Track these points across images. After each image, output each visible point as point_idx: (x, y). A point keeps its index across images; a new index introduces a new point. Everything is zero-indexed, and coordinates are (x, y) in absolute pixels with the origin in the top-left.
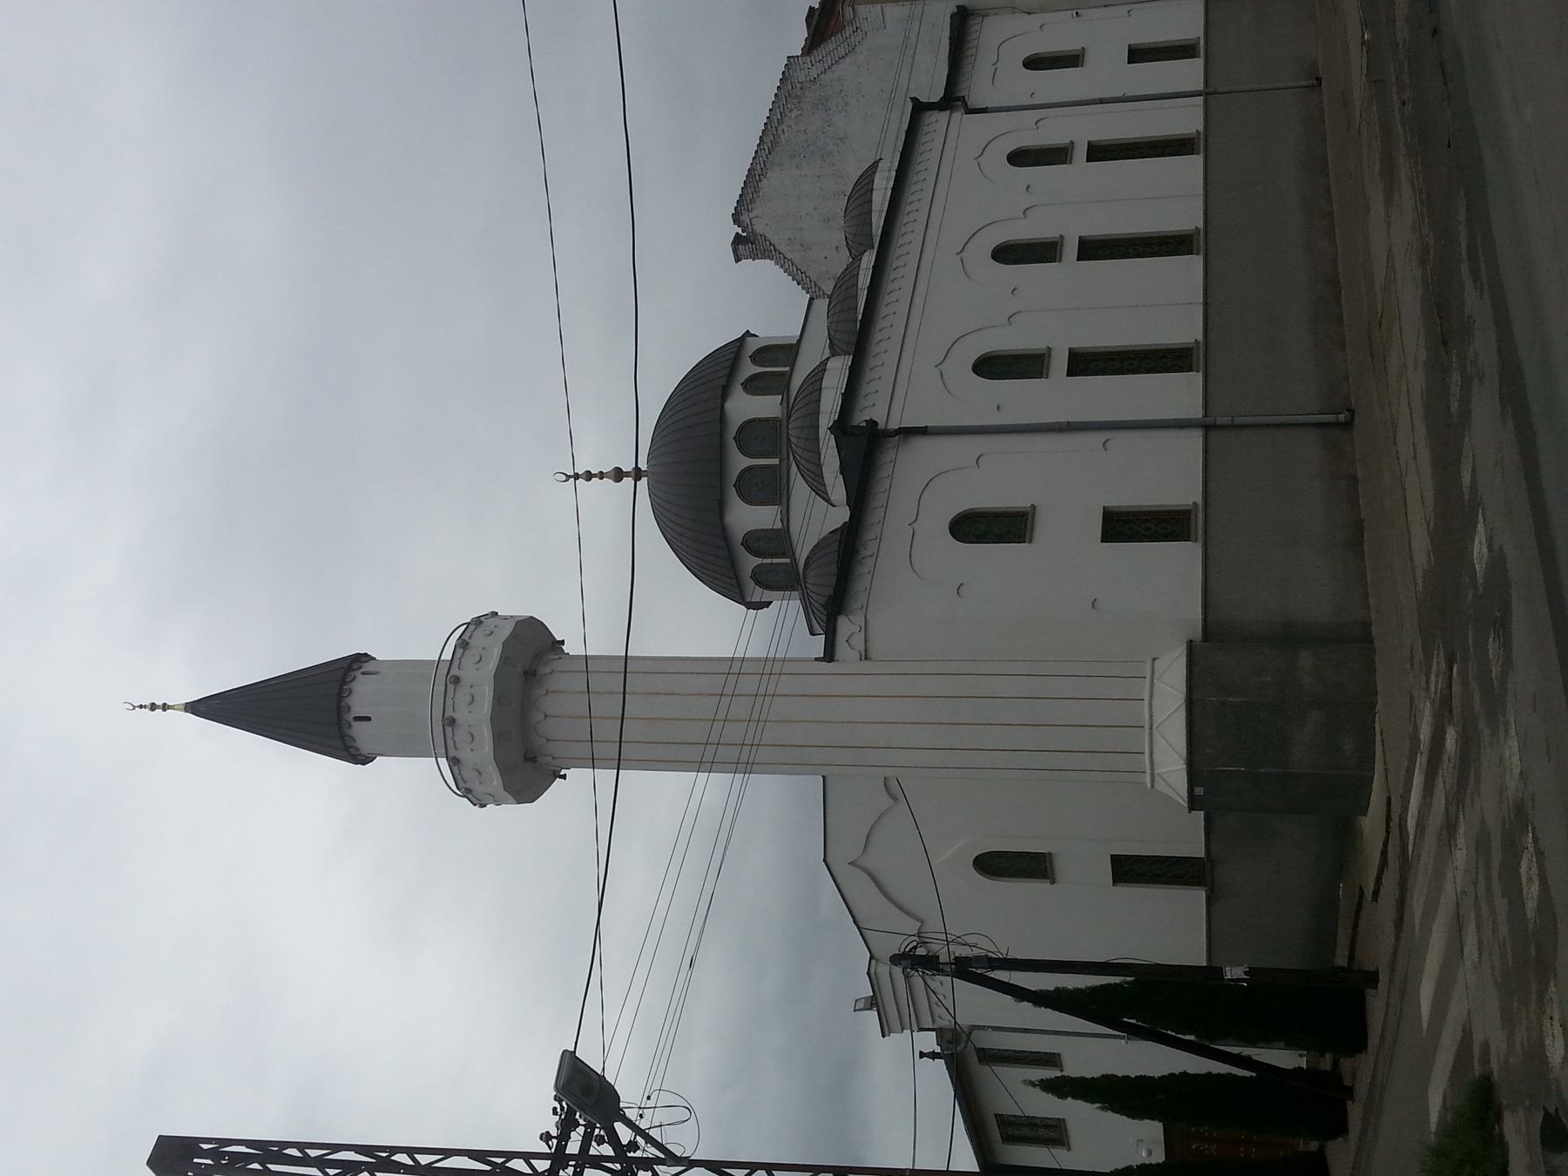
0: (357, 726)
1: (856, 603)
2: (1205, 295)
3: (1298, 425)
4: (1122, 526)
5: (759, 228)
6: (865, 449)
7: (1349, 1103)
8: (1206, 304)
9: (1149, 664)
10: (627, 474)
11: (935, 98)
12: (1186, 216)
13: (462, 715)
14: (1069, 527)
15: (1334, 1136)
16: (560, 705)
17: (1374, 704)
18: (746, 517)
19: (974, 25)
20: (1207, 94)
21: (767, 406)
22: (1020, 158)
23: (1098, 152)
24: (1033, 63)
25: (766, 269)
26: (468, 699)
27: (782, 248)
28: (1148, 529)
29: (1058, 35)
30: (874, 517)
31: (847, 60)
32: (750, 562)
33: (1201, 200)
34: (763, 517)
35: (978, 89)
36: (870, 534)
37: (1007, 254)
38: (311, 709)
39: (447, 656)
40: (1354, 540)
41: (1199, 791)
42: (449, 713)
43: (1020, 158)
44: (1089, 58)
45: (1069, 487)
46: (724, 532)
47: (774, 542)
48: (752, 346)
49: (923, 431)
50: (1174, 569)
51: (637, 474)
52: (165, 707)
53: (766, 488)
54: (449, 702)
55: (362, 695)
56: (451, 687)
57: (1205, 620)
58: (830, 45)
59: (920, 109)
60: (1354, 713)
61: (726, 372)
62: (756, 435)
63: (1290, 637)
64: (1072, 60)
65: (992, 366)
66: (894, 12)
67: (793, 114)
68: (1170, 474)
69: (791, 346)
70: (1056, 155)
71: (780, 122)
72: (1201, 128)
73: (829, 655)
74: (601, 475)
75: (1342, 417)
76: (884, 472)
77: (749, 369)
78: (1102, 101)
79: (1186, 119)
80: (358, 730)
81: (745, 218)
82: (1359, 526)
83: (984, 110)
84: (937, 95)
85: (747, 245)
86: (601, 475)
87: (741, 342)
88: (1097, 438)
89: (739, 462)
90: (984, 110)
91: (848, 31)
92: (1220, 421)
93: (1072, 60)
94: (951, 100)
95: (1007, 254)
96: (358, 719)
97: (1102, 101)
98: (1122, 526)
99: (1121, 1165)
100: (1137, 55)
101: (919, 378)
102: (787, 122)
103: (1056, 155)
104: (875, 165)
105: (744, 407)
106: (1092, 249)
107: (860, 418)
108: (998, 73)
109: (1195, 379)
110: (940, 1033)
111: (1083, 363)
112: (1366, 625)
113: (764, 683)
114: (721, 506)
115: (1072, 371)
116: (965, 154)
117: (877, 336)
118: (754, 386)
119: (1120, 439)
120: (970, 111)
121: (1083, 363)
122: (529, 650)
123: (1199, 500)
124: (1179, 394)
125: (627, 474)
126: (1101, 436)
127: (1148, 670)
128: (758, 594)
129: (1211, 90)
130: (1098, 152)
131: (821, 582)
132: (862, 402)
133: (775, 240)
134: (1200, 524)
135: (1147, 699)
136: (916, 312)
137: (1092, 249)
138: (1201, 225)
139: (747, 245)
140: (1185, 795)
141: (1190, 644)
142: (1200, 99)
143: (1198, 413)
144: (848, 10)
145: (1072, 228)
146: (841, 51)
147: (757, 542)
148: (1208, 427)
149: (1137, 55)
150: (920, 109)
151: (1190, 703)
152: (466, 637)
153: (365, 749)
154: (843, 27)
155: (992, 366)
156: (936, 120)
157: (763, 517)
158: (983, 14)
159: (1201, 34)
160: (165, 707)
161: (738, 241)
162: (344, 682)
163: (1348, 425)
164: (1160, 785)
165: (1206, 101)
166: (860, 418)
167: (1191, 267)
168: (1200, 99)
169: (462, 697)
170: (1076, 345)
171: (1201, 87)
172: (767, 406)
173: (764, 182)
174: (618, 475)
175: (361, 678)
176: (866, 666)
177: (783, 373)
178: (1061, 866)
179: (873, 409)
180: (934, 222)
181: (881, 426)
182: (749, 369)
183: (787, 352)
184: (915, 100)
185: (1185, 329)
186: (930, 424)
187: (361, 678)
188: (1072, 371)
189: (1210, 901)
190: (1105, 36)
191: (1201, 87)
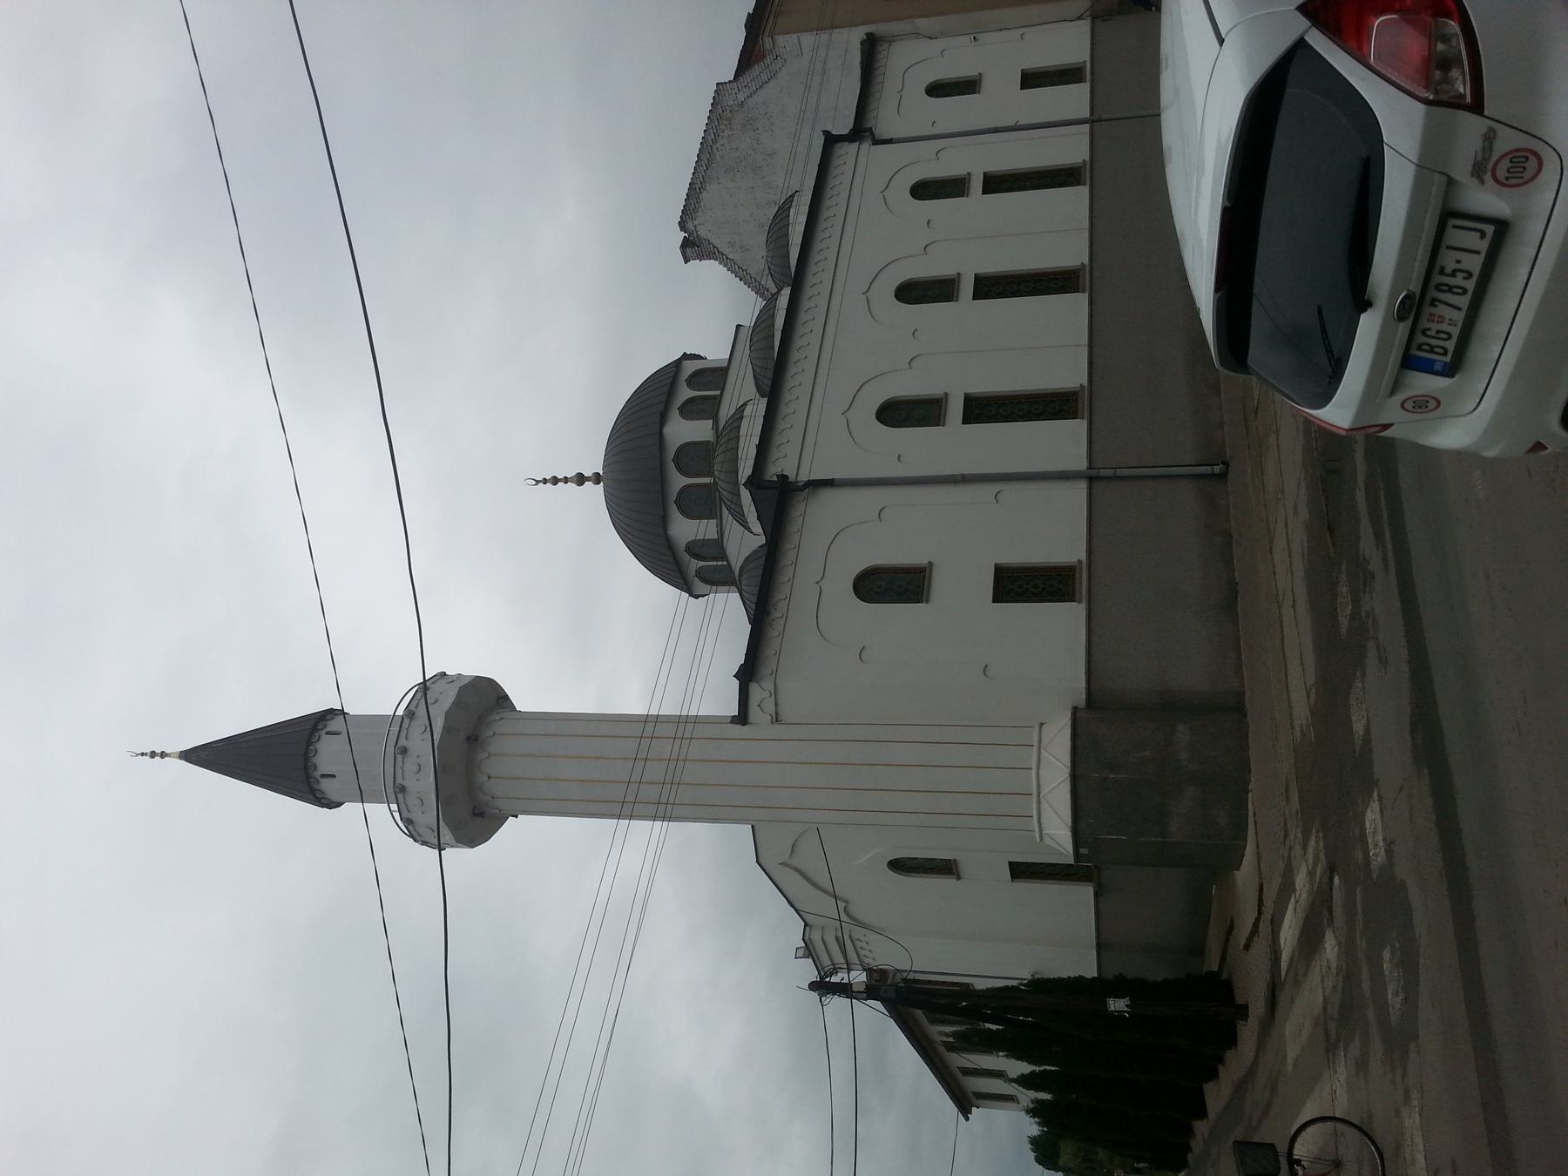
0: (324, 781)
1: (765, 671)
2: (1091, 224)
3: (1177, 476)
4: (1014, 584)
5: (703, 233)
6: (779, 499)
7: (1221, 1068)
8: (1091, 347)
9: (1036, 731)
10: (588, 479)
11: (846, 132)
12: (1070, 252)
13: (410, 783)
14: (962, 587)
15: (1209, 1080)
16: (504, 759)
17: (1248, 782)
18: (685, 529)
19: (882, 49)
20: (1092, 122)
21: (700, 430)
22: (924, 190)
23: (996, 183)
24: (937, 90)
25: (711, 270)
26: (415, 768)
27: (724, 250)
28: (1036, 586)
29: (955, 60)
30: (790, 546)
31: (771, 84)
32: (694, 565)
33: (1086, 234)
34: (703, 529)
35: (886, 121)
36: (788, 558)
37: (911, 292)
38: (284, 757)
39: (400, 712)
40: (1228, 599)
41: (1084, 851)
42: (399, 781)
43: (924, 190)
44: (987, 85)
45: (963, 541)
46: (669, 544)
47: (714, 549)
48: (690, 367)
49: (829, 483)
50: (1058, 629)
51: (597, 479)
52: (163, 755)
53: (699, 504)
54: (399, 772)
55: (329, 754)
56: (399, 758)
57: (1088, 682)
58: (756, 70)
59: (831, 140)
60: (1228, 785)
61: (666, 389)
62: (694, 457)
63: (1169, 707)
64: (968, 86)
65: (896, 413)
66: (808, 40)
67: (727, 133)
68: (1054, 530)
69: (722, 369)
70: (952, 187)
71: (715, 141)
72: (1085, 382)
73: (742, 718)
74: (566, 480)
75: (1217, 469)
76: (793, 528)
77: (685, 393)
78: (996, 130)
79: (1071, 149)
80: (325, 785)
81: (690, 225)
82: (1232, 589)
83: (890, 141)
84: (843, 126)
85: (693, 247)
86: (566, 480)
87: (677, 364)
88: (988, 490)
89: (678, 481)
90: (890, 141)
91: (769, 60)
92: (1103, 473)
93: (968, 86)
94: (860, 132)
95: (911, 292)
96: (323, 776)
97: (996, 130)
98: (1014, 584)
99: (1073, 974)
100: (1030, 80)
101: (829, 432)
102: (721, 141)
103: (952, 187)
104: (790, 199)
105: (682, 431)
106: (990, 287)
107: (772, 472)
108: (904, 107)
109: (1083, 191)
110: (869, 971)
111: (981, 409)
112: (1240, 696)
113: (684, 750)
114: (664, 520)
115: (968, 418)
116: (873, 175)
117: (792, 370)
118: (691, 410)
119: (1011, 491)
120: (877, 142)
121: (981, 409)
122: (481, 701)
123: (1083, 556)
124: (1063, 443)
125: (588, 479)
126: (992, 489)
127: (1036, 738)
128: (700, 586)
129: (1096, 117)
130: (996, 183)
131: (752, 583)
132: (775, 454)
133: (717, 243)
134: (1085, 583)
135: (1034, 767)
136: (825, 356)
137: (990, 287)
138: (1086, 261)
139: (693, 247)
140: (1071, 850)
141: (1075, 709)
142: (1086, 127)
143: (1082, 465)
144: (768, 42)
145: (967, 264)
146: (764, 77)
147: (696, 549)
148: (1092, 480)
149: (1030, 80)
150: (831, 140)
151: (1074, 778)
152: (412, 708)
153: (335, 798)
154: (764, 57)
155: (896, 413)
156: (847, 151)
157: (703, 529)
158: (891, 40)
159: (1088, 58)
160: (163, 755)
161: (686, 245)
162: (309, 743)
163: (1223, 476)
164: (1047, 841)
165: (1092, 128)
166: (772, 472)
167: (1075, 305)
168: (1086, 127)
169: (410, 766)
170: (970, 391)
171: (1086, 114)
172: (700, 430)
173: (704, 194)
174: (580, 479)
175: (325, 738)
176: (775, 730)
177: (714, 397)
178: (964, 868)
179: (784, 463)
180: (834, 308)
181: (792, 478)
182: (685, 393)
183: (714, 376)
184: (827, 134)
185: (1068, 373)
186: (836, 476)
187: (325, 738)
188: (968, 418)
189: (1096, 895)
190: (999, 54)
191: (1086, 114)
